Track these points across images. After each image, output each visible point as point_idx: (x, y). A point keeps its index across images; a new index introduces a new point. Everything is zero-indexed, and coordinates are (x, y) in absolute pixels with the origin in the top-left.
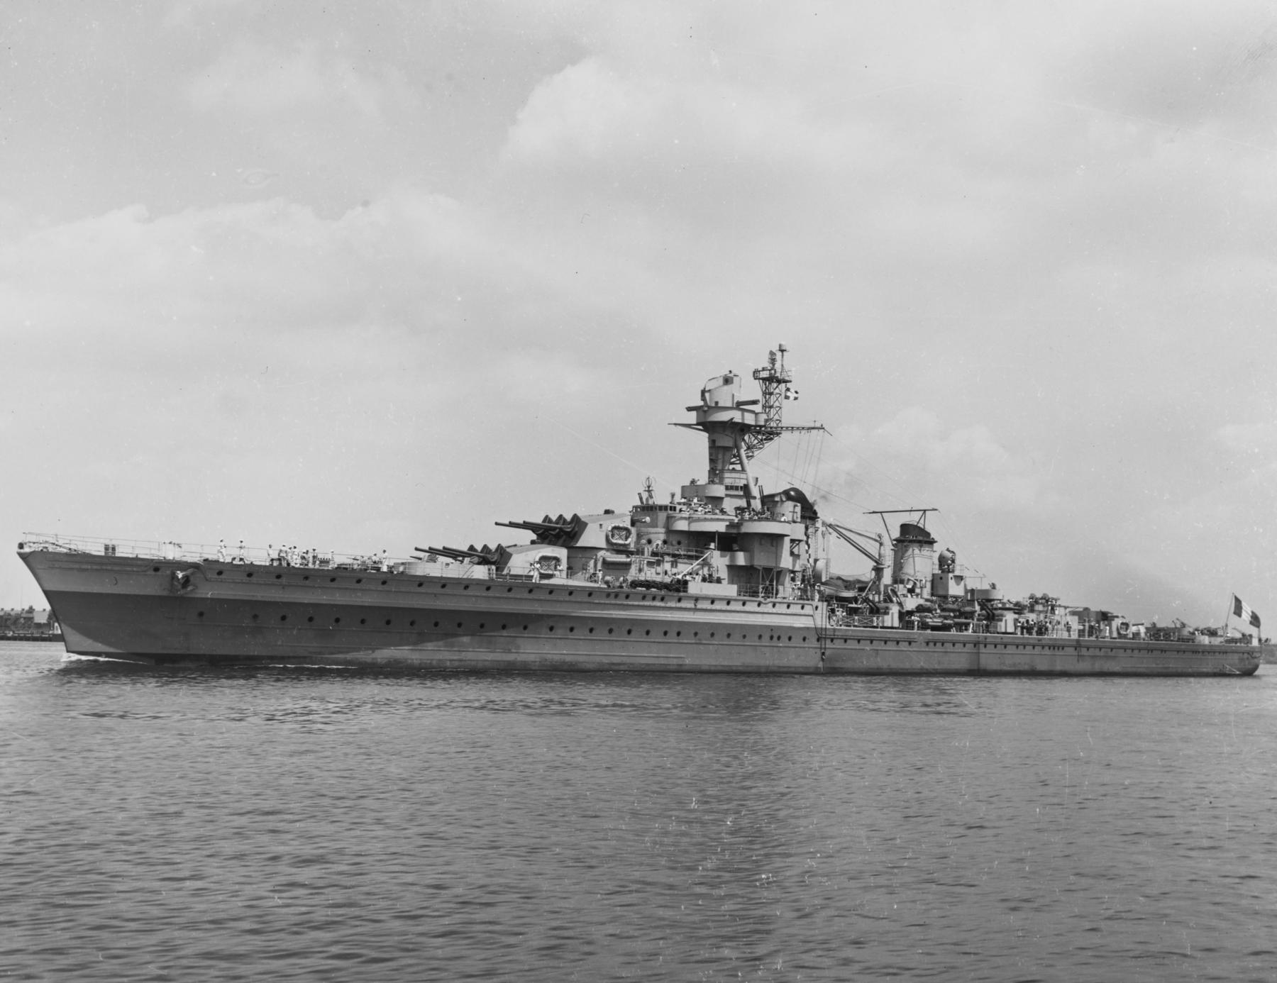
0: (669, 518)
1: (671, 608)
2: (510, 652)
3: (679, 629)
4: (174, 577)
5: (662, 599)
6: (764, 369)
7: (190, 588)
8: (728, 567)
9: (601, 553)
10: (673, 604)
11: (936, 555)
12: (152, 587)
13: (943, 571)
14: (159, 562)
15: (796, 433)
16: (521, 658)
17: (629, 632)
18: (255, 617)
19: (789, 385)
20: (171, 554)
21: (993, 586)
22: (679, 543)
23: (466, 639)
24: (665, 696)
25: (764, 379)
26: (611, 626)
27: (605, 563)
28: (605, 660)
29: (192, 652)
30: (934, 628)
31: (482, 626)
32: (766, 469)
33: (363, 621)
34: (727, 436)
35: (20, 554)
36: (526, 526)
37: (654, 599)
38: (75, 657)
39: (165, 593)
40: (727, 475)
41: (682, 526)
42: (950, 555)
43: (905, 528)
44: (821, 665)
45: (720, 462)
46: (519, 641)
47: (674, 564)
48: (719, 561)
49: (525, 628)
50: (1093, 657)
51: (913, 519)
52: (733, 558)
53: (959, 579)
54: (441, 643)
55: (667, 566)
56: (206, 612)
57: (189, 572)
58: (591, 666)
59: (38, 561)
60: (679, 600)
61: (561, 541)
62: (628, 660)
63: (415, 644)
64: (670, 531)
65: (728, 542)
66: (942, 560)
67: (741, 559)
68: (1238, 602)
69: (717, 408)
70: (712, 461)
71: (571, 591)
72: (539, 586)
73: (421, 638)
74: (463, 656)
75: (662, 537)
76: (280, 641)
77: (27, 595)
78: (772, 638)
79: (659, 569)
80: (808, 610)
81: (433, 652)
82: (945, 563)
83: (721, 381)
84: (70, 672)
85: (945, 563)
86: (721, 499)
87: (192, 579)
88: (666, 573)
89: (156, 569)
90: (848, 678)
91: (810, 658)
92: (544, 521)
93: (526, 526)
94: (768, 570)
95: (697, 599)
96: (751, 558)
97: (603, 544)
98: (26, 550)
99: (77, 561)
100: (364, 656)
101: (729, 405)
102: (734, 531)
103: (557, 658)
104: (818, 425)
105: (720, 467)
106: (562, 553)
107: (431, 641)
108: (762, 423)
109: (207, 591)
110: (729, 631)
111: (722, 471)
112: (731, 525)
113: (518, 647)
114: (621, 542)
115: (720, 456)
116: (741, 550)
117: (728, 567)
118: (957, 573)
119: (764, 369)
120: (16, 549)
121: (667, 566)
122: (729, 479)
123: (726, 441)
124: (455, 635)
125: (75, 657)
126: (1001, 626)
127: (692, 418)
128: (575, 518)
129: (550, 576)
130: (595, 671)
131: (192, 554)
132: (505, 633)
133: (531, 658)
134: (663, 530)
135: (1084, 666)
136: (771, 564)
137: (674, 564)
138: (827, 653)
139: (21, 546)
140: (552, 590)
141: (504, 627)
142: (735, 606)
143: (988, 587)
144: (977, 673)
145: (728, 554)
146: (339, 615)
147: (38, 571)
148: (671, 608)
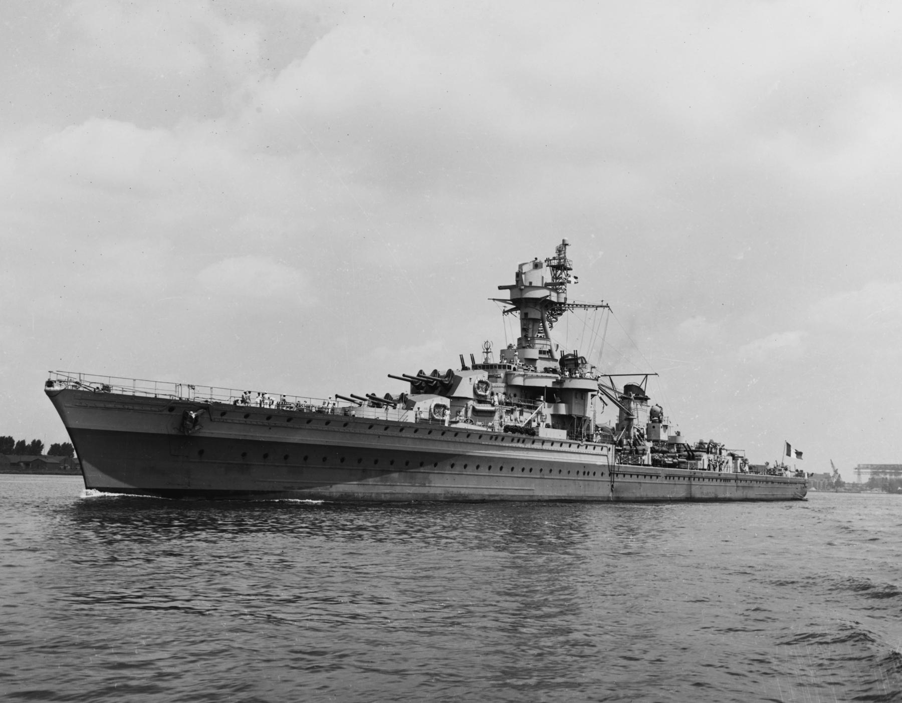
0: (507, 375)
1: (528, 449)
2: (424, 486)
3: (529, 467)
4: (186, 416)
5: (523, 442)
6: (554, 259)
7: (197, 428)
8: (552, 415)
9: (470, 403)
10: (529, 446)
11: (649, 409)
12: (163, 426)
13: (653, 422)
14: (175, 402)
15: (591, 310)
16: (432, 491)
17: (501, 468)
18: (244, 455)
19: (569, 272)
20: (186, 394)
21: (678, 434)
22: (515, 396)
23: (395, 475)
24: (472, 518)
25: (553, 267)
26: (490, 463)
27: (474, 410)
28: (486, 492)
29: (192, 487)
30: (670, 466)
31: (407, 464)
32: (563, 335)
33: (324, 459)
34: (535, 308)
35: (49, 393)
36: (405, 378)
37: (518, 441)
38: (96, 494)
39: (174, 432)
40: (537, 341)
41: (518, 381)
42: (658, 409)
43: (628, 388)
44: (611, 495)
45: (530, 331)
46: (431, 476)
47: (521, 413)
48: (547, 410)
49: (436, 465)
50: (743, 487)
51: (637, 381)
52: (556, 409)
53: (666, 427)
54: (378, 479)
55: (517, 413)
56: (206, 449)
57: (201, 411)
58: (476, 498)
59: (63, 398)
60: (533, 443)
61: (438, 391)
62: (500, 492)
63: (360, 480)
64: (509, 386)
65: (554, 395)
66: (653, 413)
67: (563, 409)
68: (789, 446)
69: (531, 287)
70: (524, 330)
71: (469, 434)
72: (449, 429)
73: (364, 474)
74: (398, 489)
75: (503, 390)
76: (258, 478)
77: (53, 432)
78: (584, 473)
79: (513, 417)
80: (605, 451)
81: (373, 487)
82: (656, 416)
83: (531, 266)
84: (85, 511)
85: (656, 416)
86: (535, 360)
87: (199, 419)
88: (516, 420)
89: (171, 409)
90: (628, 506)
91: (604, 491)
92: (418, 375)
93: (405, 378)
94: (579, 418)
95: (543, 442)
96: (569, 408)
97: (471, 395)
98: (57, 388)
99: (103, 399)
100: (340, 489)
101: (540, 285)
102: (558, 387)
103: (455, 491)
104: (604, 304)
105: (530, 335)
106: (446, 401)
107: (370, 477)
108: (563, 301)
109: (210, 431)
110: (561, 468)
111: (533, 338)
112: (558, 382)
113: (430, 482)
114: (483, 394)
115: (531, 326)
116: (562, 402)
117: (552, 415)
118: (664, 423)
119: (554, 259)
120: (43, 386)
121: (517, 413)
122: (540, 344)
123: (535, 314)
124: (389, 472)
125: (96, 494)
126: (700, 465)
127: (506, 294)
128: (450, 372)
129: (457, 422)
130: (546, 501)
131: (224, 392)
132: (422, 470)
133: (439, 491)
134: (503, 385)
135: (739, 494)
136: (581, 414)
137: (521, 413)
138: (615, 485)
139: (50, 383)
140: (457, 432)
141: (422, 465)
142: (565, 448)
143: (674, 435)
144: (690, 500)
145: (553, 405)
146: (307, 452)
147: (68, 412)
148: (528, 449)
